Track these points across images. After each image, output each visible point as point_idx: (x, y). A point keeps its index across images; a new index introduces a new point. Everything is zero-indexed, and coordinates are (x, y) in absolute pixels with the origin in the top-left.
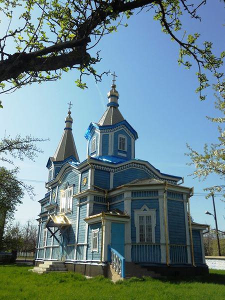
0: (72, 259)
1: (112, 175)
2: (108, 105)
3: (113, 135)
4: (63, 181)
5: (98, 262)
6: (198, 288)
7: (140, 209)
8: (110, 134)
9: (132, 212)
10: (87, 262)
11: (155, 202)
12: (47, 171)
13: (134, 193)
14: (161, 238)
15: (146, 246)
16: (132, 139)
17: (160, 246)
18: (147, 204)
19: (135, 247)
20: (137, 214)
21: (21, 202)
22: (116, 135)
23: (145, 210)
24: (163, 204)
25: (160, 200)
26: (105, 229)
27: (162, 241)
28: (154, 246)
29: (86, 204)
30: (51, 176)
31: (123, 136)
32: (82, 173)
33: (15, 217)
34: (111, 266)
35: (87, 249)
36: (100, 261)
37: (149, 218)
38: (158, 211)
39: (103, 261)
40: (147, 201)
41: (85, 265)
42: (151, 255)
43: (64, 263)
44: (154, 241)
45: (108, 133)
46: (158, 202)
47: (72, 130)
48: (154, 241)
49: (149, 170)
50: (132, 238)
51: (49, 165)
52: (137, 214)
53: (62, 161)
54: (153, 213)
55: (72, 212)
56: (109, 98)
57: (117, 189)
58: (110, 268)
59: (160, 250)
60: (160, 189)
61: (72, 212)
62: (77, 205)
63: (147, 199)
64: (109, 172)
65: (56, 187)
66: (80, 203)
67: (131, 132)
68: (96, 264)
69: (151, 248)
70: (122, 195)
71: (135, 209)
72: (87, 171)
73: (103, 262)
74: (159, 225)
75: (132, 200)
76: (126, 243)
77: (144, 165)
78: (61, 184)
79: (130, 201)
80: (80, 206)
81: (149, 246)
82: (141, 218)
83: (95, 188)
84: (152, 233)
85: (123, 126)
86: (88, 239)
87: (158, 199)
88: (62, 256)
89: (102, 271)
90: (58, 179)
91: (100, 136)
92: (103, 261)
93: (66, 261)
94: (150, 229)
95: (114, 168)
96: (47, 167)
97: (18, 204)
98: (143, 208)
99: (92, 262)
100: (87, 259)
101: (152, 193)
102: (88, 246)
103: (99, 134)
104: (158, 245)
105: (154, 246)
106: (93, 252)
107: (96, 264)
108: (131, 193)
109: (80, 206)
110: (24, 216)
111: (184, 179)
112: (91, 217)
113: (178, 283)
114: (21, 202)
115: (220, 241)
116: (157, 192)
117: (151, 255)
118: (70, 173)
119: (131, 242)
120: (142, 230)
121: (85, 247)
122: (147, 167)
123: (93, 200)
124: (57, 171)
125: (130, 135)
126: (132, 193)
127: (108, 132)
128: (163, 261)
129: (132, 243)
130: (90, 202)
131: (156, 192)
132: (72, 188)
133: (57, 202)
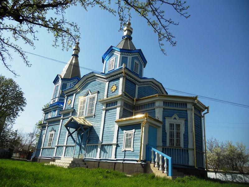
0: (96, 155)
1: (137, 86)
2: (72, 55)
3: (131, 58)
4: (82, 89)
5: (137, 161)
6: (204, 182)
7: (171, 117)
8: (68, 83)
9: (164, 118)
10: (117, 160)
11: (183, 113)
12: (54, 86)
13: (165, 103)
14: (189, 143)
15: (175, 149)
16: (143, 66)
17: (187, 150)
18: (177, 113)
19: (170, 151)
20: (168, 121)
21: (23, 110)
22: (133, 59)
23: (175, 118)
24: (191, 115)
25: (189, 112)
26: (144, 130)
27: (190, 146)
28: (182, 150)
29: (116, 108)
30: (57, 90)
31: (137, 62)
32: (110, 82)
33: (15, 122)
34: (152, 165)
35: (116, 148)
36: (138, 159)
37: (178, 126)
38: (186, 121)
39: (141, 159)
40: (177, 111)
41: (115, 163)
42: (180, 158)
43: (83, 161)
44: (182, 145)
45: (127, 56)
46: (187, 113)
47: (78, 57)
48: (182, 145)
49: (160, 91)
50: (163, 141)
51: (55, 81)
52: (168, 121)
53: (69, 79)
54: (182, 122)
55: (95, 115)
56: (74, 50)
57: (141, 99)
58: (149, 167)
59: (188, 154)
60: (189, 102)
61: (95, 115)
62: (103, 110)
63: (177, 110)
64: (135, 84)
65: (73, 95)
66: (42, 128)
67: (143, 60)
68: (136, 162)
69: (175, 152)
70: (153, 103)
71: (166, 116)
72: (118, 79)
73: (141, 161)
74: (188, 133)
75: (164, 109)
76: (157, 146)
77: (158, 86)
78: (79, 92)
79: (162, 109)
80: (107, 110)
81: (178, 149)
82: (171, 125)
83: (125, 94)
84: (169, 138)
85: (77, 79)
86: (117, 139)
87: (186, 111)
88: (79, 154)
89: (141, 169)
90: (77, 87)
91: (120, 57)
92: (141, 159)
93: (85, 159)
94: (178, 134)
95: (141, 82)
96: (54, 82)
97: (21, 111)
98: (173, 117)
99: (124, 160)
100: (116, 158)
101: (182, 105)
102: (117, 146)
103: (119, 55)
104: (186, 150)
105: (182, 150)
106: (125, 151)
107: (136, 162)
108: (163, 103)
109: (107, 110)
110: (24, 125)
111: (210, 109)
112: (120, 120)
113: (202, 179)
114: (23, 110)
115: (124, 155)
116: (186, 104)
117: (180, 158)
118: (93, 82)
119: (162, 145)
120: (171, 135)
121: (114, 147)
122: (160, 90)
123: (123, 105)
124: (64, 87)
125: (142, 62)
126: (164, 102)
127: (128, 55)
128: (191, 163)
129: (163, 146)
130: (121, 106)
131: (185, 104)
132: (96, 94)
133: (73, 107)
